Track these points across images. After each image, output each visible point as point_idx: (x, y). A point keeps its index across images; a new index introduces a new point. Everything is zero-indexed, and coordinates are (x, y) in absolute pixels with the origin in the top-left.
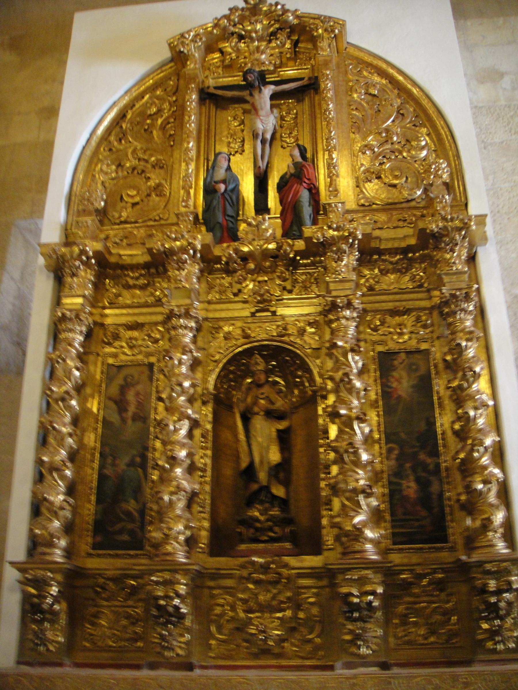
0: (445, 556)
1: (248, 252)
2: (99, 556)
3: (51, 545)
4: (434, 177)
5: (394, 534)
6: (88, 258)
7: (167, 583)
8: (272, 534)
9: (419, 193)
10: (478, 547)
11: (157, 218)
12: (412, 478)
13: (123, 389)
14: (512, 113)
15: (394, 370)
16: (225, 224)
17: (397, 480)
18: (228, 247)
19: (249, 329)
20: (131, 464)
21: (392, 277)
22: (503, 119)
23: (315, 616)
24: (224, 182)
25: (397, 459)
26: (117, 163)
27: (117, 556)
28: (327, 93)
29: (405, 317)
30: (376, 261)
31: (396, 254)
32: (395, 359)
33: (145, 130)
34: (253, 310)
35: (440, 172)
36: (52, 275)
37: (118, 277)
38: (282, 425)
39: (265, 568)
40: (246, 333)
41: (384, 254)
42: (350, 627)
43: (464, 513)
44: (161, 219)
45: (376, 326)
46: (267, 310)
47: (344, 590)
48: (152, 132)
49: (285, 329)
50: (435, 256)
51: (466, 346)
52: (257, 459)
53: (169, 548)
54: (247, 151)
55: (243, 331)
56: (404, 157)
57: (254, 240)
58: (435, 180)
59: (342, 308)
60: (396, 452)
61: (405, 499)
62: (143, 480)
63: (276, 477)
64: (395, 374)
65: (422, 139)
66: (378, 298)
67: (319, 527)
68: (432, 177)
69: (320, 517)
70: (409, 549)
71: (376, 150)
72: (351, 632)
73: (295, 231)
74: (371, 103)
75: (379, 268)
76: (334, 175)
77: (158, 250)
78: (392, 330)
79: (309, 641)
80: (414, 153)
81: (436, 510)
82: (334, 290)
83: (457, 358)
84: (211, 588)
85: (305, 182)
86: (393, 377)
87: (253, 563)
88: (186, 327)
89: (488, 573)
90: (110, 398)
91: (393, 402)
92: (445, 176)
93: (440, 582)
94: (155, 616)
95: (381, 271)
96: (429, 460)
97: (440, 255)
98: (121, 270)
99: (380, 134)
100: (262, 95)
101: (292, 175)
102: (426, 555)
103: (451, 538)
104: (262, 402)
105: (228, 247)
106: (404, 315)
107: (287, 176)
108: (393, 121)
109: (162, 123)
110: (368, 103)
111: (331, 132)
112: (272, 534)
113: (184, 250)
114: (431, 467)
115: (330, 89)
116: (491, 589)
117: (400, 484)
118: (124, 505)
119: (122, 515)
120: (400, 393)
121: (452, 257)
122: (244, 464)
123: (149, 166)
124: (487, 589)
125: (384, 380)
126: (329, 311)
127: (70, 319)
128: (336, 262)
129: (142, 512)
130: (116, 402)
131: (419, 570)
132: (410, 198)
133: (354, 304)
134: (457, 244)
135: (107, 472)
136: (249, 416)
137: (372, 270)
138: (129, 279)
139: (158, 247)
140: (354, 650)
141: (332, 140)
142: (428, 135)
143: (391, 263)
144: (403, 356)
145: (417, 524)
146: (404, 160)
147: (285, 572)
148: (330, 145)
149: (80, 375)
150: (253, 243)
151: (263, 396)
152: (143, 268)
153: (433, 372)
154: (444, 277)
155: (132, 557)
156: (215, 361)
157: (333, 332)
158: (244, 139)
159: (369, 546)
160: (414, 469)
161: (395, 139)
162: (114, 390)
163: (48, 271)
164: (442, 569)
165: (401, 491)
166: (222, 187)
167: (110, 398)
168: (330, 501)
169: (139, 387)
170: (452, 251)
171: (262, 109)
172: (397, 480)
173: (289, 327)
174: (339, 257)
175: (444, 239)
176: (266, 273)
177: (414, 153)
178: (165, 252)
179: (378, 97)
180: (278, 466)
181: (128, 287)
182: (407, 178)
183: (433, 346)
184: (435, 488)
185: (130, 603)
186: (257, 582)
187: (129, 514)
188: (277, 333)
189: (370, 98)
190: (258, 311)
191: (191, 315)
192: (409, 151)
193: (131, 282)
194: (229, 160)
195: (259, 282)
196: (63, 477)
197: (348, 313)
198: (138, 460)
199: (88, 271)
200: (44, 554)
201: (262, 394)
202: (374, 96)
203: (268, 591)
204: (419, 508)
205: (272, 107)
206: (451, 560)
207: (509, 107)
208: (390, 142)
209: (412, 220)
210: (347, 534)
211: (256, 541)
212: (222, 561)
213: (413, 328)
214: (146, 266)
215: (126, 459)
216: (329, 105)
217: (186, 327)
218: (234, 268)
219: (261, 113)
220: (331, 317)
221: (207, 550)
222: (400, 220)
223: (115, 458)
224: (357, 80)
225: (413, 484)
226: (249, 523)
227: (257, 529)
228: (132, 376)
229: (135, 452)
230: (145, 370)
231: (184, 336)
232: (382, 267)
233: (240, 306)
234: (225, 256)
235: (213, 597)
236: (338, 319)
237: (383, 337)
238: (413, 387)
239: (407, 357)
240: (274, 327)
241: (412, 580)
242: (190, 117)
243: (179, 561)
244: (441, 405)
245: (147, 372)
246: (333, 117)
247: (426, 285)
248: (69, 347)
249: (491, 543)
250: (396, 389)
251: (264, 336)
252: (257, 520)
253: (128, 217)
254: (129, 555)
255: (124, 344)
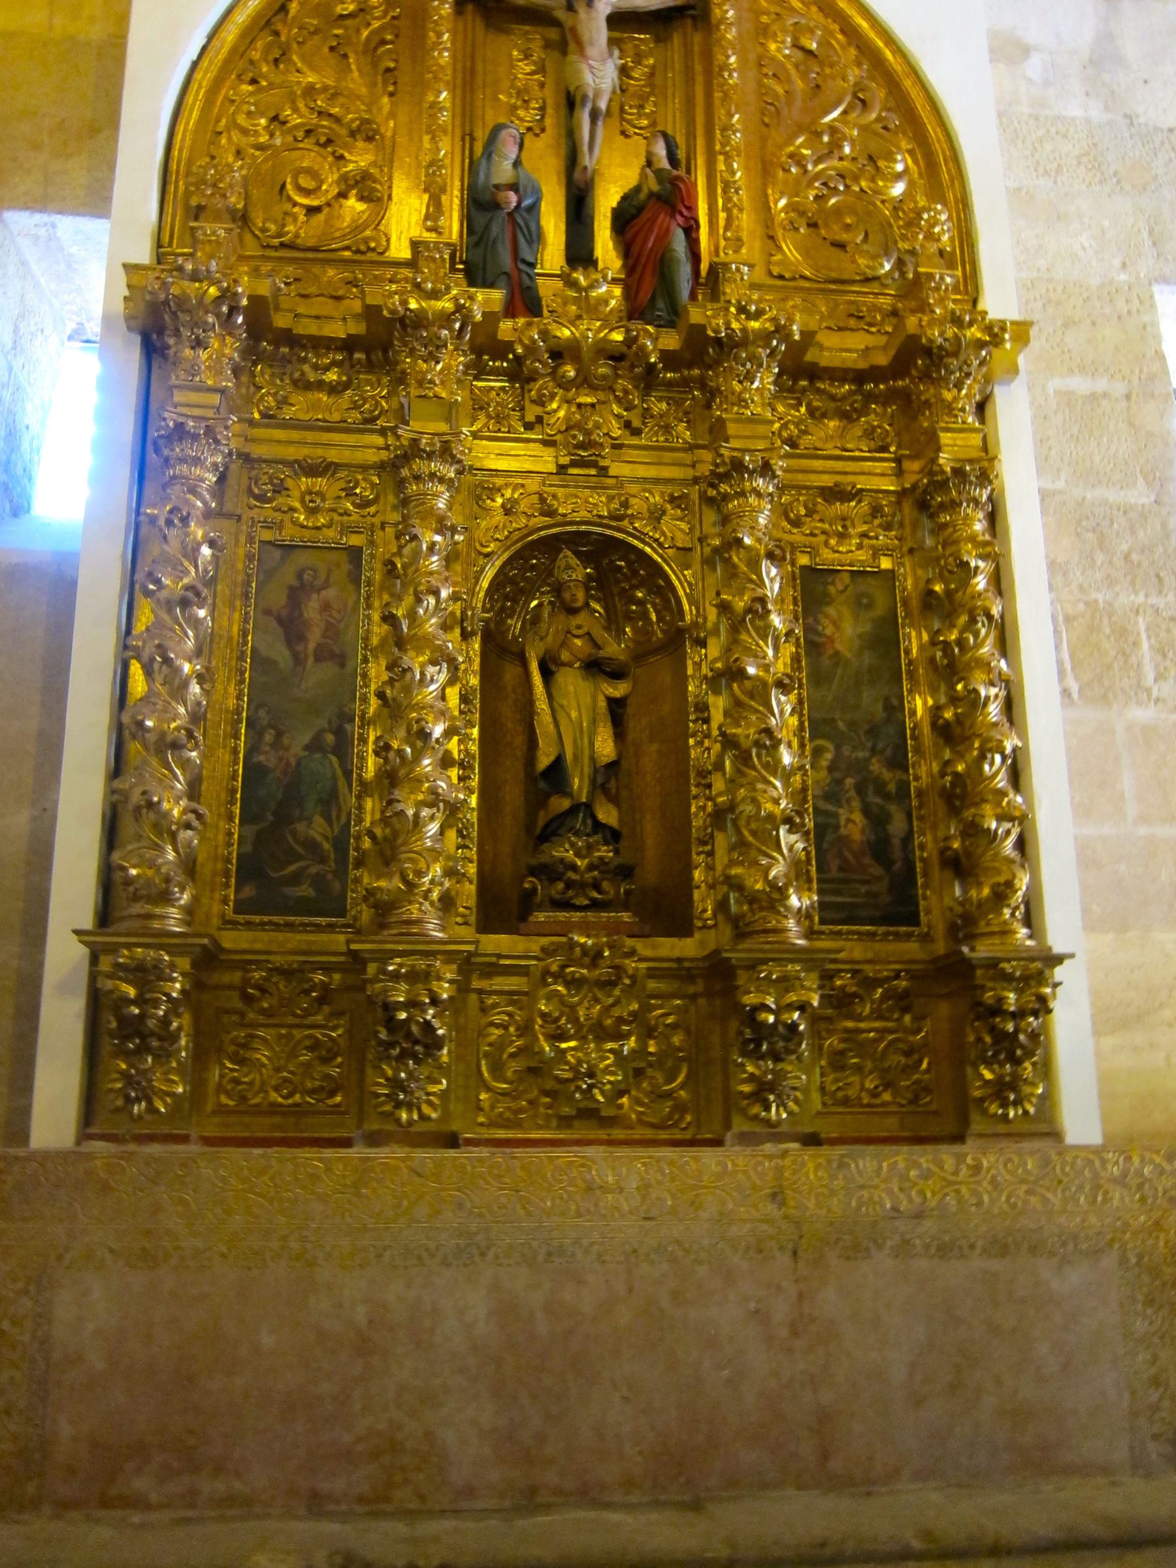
0: (687, 947)
1: (568, 340)
2: (249, 925)
3: (165, 898)
4: (925, 237)
5: (823, 905)
6: (233, 310)
7: (414, 977)
8: (595, 895)
9: (887, 267)
10: (984, 934)
11: (363, 248)
12: (856, 804)
13: (297, 594)
14: (1040, 133)
15: (829, 603)
16: (515, 275)
17: (830, 807)
18: (529, 324)
19: (554, 496)
20: (315, 746)
21: (832, 424)
22: (1023, 142)
23: (680, 1050)
24: (514, 187)
25: (831, 769)
26: (272, 114)
27: (290, 926)
28: (725, 30)
29: (853, 504)
30: (804, 390)
31: (843, 381)
32: (833, 583)
33: (332, 49)
34: (565, 460)
35: (937, 230)
36: (137, 339)
37: (286, 361)
38: (619, 690)
39: (595, 957)
40: (549, 506)
41: (820, 378)
42: (750, 1069)
43: (948, 874)
44: (370, 249)
45: (798, 517)
46: (594, 465)
47: (750, 999)
48: (345, 56)
49: (625, 505)
50: (921, 393)
51: (977, 568)
52: (569, 756)
53: (414, 911)
54: (549, 130)
55: (543, 500)
56: (862, 190)
57: (579, 317)
58: (927, 245)
59: (751, 473)
60: (829, 756)
61: (844, 841)
62: (342, 783)
63: (604, 788)
64: (831, 611)
65: (899, 157)
66: (804, 463)
67: (687, 885)
68: (921, 237)
69: (689, 867)
70: (849, 933)
71: (810, 167)
72: (752, 1078)
73: (660, 310)
74: (802, 68)
75: (808, 406)
76: (735, 205)
77: (393, 312)
78: (826, 526)
79: (669, 1095)
80: (881, 183)
81: (898, 865)
82: (737, 437)
83: (956, 590)
84: (480, 992)
85: (682, 214)
86: (827, 616)
87: (572, 945)
88: (441, 480)
89: (1008, 978)
90: (268, 612)
91: (826, 662)
92: (945, 238)
93: (906, 994)
94: (381, 1043)
95: (811, 411)
96: (887, 775)
97: (932, 391)
98: (291, 348)
99: (819, 135)
100: (594, 14)
101: (652, 194)
102: (878, 946)
103: (923, 918)
104: (578, 642)
105: (529, 324)
106: (850, 501)
107: (643, 196)
108: (845, 112)
109: (368, 38)
110: (797, 66)
111: (732, 116)
112: (595, 895)
113: (446, 319)
114: (892, 788)
115: (731, 24)
116: (1012, 1009)
117: (836, 815)
118: (301, 827)
119: (300, 850)
120: (838, 646)
121: (956, 399)
122: (544, 761)
123: (344, 132)
124: (1005, 1007)
125: (810, 620)
126: (725, 477)
127: (195, 437)
128: (740, 382)
129: (341, 844)
130: (280, 621)
131: (869, 970)
132: (870, 273)
133: (775, 467)
134: (968, 375)
135: (267, 758)
136: (553, 668)
137: (796, 407)
138: (306, 368)
139: (393, 304)
140: (756, 1109)
141: (734, 133)
142: (911, 152)
143: (833, 398)
144: (846, 578)
145: (864, 889)
146: (864, 195)
147: (631, 964)
148: (728, 143)
149: (213, 555)
150: (578, 322)
151: (580, 632)
152: (339, 349)
153: (900, 612)
154: (942, 435)
155: (319, 928)
156: (487, 555)
157: (725, 520)
158: (544, 102)
159: (791, 923)
160: (860, 789)
161: (847, 150)
162: (278, 598)
163: (129, 328)
164: (907, 971)
165: (837, 827)
166: (513, 198)
167: (268, 612)
168: (712, 836)
169: (331, 593)
170: (959, 385)
171: (592, 44)
172: (830, 807)
173: (633, 501)
174: (748, 372)
175: (950, 360)
176: (593, 388)
177: (881, 183)
178: (402, 320)
179: (816, 56)
180: (613, 766)
181: (304, 385)
182: (866, 234)
183: (903, 564)
184: (897, 826)
185: (319, 1019)
186: (573, 983)
187: (312, 846)
188: (609, 512)
189: (800, 55)
190: (574, 464)
191: (453, 456)
192: (873, 180)
193: (312, 377)
194: (521, 146)
195: (579, 406)
196: (185, 764)
197: (760, 483)
198: (330, 738)
199: (228, 339)
200: (150, 916)
201: (579, 627)
202: (810, 53)
203: (597, 1000)
204: (867, 860)
205: (612, 42)
206: (922, 956)
207: (1037, 119)
208: (836, 156)
209: (875, 317)
210: (752, 899)
211: (567, 906)
212: (497, 943)
213: (865, 528)
214: (349, 345)
215: (306, 738)
216: (728, 57)
217: (441, 480)
218: (536, 371)
219: (591, 52)
220: (724, 488)
221: (473, 919)
222: (852, 315)
223: (279, 734)
224: (777, 14)
225: (858, 817)
226: (550, 872)
227: (569, 885)
228: (315, 571)
229: (324, 724)
230: (343, 557)
231: (436, 495)
232: (815, 404)
233: (537, 449)
234: (521, 342)
235: (484, 1010)
236: (742, 494)
237: (811, 539)
238: (860, 636)
239: (852, 581)
240: (603, 499)
241: (854, 989)
242: (439, 35)
243: (794, 944)
244: (911, 675)
245: (346, 567)
246: (736, 85)
247: (892, 449)
248: (190, 497)
249: (1007, 928)
250: (831, 640)
251: (583, 514)
252: (573, 867)
253: (297, 236)
254: (317, 925)
255: (297, 505)
